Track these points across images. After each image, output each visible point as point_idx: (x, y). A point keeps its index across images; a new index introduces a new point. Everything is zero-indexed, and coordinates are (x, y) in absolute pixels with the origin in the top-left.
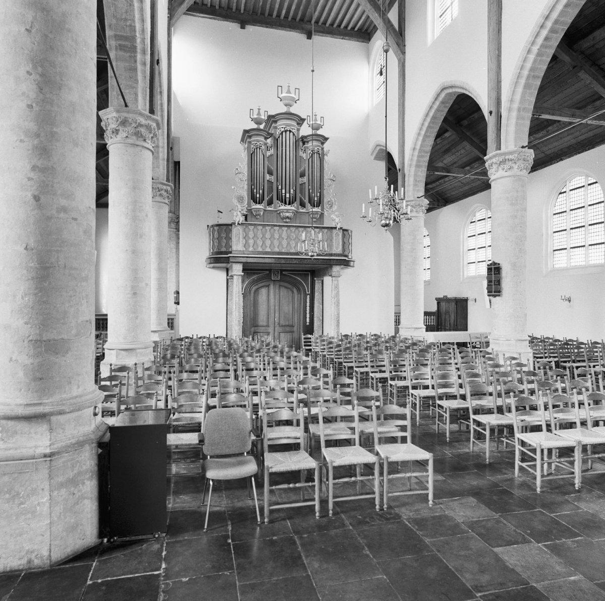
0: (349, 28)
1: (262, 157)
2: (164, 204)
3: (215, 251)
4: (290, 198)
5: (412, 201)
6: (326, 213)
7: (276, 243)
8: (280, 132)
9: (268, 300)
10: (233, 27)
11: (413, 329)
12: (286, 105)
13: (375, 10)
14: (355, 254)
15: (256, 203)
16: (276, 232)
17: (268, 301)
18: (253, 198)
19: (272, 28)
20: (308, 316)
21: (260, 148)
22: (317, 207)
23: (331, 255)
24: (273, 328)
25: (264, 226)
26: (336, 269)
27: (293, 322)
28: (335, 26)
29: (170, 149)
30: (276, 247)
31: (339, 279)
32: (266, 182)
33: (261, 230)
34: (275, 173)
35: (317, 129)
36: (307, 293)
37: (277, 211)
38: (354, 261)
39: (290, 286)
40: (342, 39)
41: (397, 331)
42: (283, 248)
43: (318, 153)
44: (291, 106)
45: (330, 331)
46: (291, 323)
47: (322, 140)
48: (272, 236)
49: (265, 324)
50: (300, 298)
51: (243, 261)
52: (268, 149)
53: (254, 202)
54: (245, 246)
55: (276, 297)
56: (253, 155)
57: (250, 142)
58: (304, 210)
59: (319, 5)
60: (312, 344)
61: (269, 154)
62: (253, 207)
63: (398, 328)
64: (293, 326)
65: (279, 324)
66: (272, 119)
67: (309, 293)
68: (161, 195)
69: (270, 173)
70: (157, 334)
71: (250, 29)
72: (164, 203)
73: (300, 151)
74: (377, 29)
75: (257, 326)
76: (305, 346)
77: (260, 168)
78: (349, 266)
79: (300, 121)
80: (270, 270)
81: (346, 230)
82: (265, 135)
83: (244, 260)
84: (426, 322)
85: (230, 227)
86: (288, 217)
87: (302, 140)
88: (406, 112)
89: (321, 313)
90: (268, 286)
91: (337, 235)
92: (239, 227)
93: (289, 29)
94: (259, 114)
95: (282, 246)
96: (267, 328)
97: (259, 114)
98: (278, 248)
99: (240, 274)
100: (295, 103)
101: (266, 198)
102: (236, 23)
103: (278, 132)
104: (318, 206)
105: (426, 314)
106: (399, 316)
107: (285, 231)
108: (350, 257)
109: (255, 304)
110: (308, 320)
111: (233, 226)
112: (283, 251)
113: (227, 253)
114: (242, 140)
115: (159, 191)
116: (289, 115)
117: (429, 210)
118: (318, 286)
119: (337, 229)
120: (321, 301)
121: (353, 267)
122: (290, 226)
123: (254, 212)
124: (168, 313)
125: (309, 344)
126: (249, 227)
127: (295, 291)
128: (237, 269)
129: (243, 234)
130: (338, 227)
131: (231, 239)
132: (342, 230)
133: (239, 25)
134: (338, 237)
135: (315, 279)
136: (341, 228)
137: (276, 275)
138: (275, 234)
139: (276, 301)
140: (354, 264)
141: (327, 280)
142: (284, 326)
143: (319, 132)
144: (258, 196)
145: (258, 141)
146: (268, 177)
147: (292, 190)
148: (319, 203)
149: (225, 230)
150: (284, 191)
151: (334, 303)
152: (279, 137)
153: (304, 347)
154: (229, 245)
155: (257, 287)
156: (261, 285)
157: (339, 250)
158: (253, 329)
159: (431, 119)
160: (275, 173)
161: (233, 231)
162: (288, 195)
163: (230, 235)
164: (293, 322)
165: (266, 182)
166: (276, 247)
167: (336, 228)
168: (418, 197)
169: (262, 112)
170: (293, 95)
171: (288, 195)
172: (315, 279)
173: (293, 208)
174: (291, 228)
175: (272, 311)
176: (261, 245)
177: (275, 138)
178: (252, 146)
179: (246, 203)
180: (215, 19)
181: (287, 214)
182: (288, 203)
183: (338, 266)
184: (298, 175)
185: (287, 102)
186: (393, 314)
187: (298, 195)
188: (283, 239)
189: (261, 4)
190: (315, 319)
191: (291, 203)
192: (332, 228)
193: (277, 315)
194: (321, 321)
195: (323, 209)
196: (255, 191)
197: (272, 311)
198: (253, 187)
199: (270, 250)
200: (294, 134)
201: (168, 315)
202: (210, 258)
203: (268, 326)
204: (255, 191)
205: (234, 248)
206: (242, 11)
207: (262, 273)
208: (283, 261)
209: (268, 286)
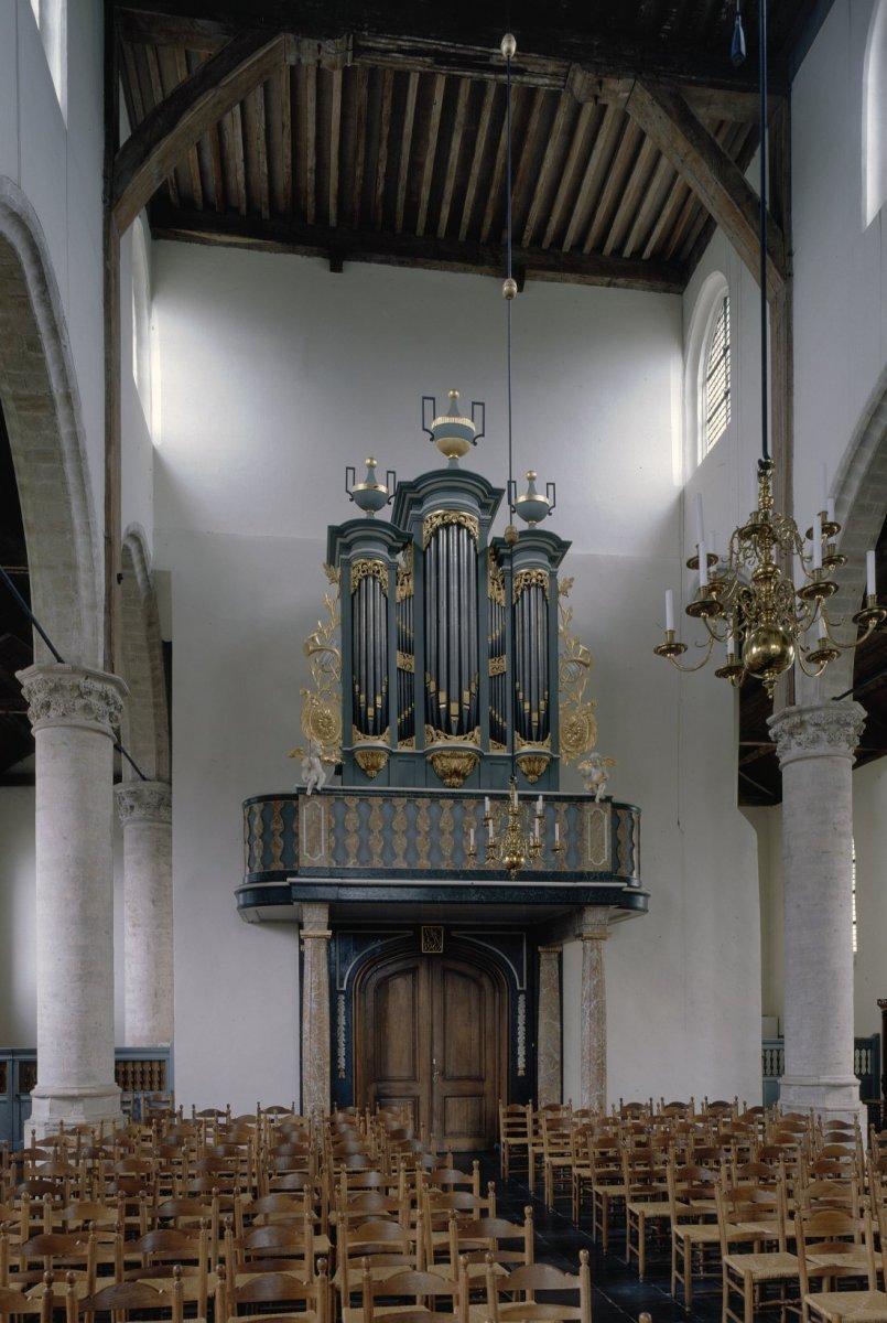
0: (627, 252)
1: (381, 601)
2: (98, 736)
3: (256, 870)
4: (460, 715)
5: (818, 709)
6: (564, 762)
7: (423, 845)
8: (431, 530)
9: (414, 1008)
10: (311, 267)
11: (823, 1089)
12: (447, 452)
13: (702, 154)
14: (647, 877)
15: (367, 732)
16: (423, 811)
17: (414, 1011)
18: (358, 719)
19: (414, 265)
20: (521, 1051)
21: (374, 578)
22: (538, 740)
23: (581, 876)
24: (426, 1086)
25: (388, 796)
26: (594, 917)
27: (481, 1069)
28: (587, 248)
29: (115, 579)
30: (423, 854)
31: (603, 944)
32: (394, 672)
33: (381, 807)
34: (418, 648)
35: (539, 519)
36: (518, 988)
37: (424, 755)
38: (646, 895)
39: (471, 971)
40: (609, 285)
41: (772, 1095)
42: (442, 857)
43: (539, 586)
44: (461, 453)
45: (578, 1094)
46: (474, 1072)
47: (551, 549)
48: (412, 827)
49: (405, 1074)
50: (501, 1005)
51: (330, 897)
52: (396, 580)
53: (360, 729)
54: (333, 856)
55: (435, 1004)
56: (356, 597)
57: (347, 564)
58: (504, 752)
59: (541, 180)
60: (507, 1130)
61: (403, 594)
62: (359, 744)
63: (777, 1086)
64: (480, 1079)
65: (443, 1073)
66: (409, 495)
67: (525, 988)
68: (87, 708)
69: (406, 647)
70: (80, 1107)
71: (356, 270)
72: (98, 731)
73: (490, 585)
74: (716, 224)
75: (385, 1079)
76: (509, 1135)
77: (376, 629)
78: (635, 908)
79: (489, 498)
80: (416, 928)
81: (625, 807)
82: (390, 541)
83: (330, 894)
84: (860, 1066)
85: (295, 803)
86: (456, 773)
87: (496, 552)
88: (796, 450)
89: (558, 1043)
90: (414, 971)
91: (597, 818)
92: (317, 801)
93: (460, 265)
94: (371, 479)
95: (440, 850)
96: (411, 1084)
97: (371, 479)
98: (429, 859)
99: (320, 933)
100: (471, 446)
101: (396, 720)
102: (317, 255)
103: (427, 529)
104: (541, 736)
105: (860, 1044)
106: (778, 1051)
107: (446, 809)
108: (635, 883)
109: (380, 1019)
110: (521, 1063)
111: (301, 797)
112: (443, 867)
113: (282, 876)
114: (331, 560)
115: (81, 696)
116: (455, 480)
117: (855, 767)
118: (546, 970)
119: (597, 800)
120: (557, 1011)
121: (645, 910)
122: (461, 796)
123: (359, 759)
124: (118, 1045)
125: (521, 1130)
126: (347, 799)
127: (486, 982)
128: (316, 921)
129: (330, 821)
130: (600, 793)
131: (297, 835)
132: (609, 805)
133: (327, 262)
134: (598, 825)
135: (540, 949)
136: (608, 799)
137: (432, 939)
138: (419, 820)
139: (435, 1013)
140: (646, 903)
141: (573, 951)
142: (459, 1079)
143: (540, 526)
144: (371, 711)
145: (370, 557)
146: (399, 659)
147: (466, 695)
148: (545, 729)
149: (281, 812)
150: (443, 697)
151: (591, 1015)
152: (429, 545)
153: (503, 1139)
154: (290, 853)
155: (381, 974)
156: (392, 969)
157: (603, 862)
158: (372, 1089)
159: (878, 451)
160: (418, 648)
161: (300, 811)
162: (454, 708)
163: (295, 825)
164: (481, 1069)
165: (394, 672)
166: (423, 854)
167: (591, 799)
168: (834, 699)
169: (380, 475)
170: (467, 422)
171: (454, 708)
172: (540, 949)
173: (471, 745)
174: (465, 802)
175: (425, 1041)
176: (379, 851)
177: (417, 548)
178: (354, 573)
179: (339, 734)
180: (259, 248)
181: (455, 764)
182: (454, 729)
183: (599, 908)
184: (485, 653)
185: (450, 440)
186: (759, 1047)
187: (486, 709)
188: (442, 832)
189: (381, 190)
190: (542, 1060)
191: (465, 730)
192: (582, 799)
193: (437, 1050)
194: (558, 1066)
195: (555, 747)
196: (363, 697)
197: (425, 1041)
198: (357, 686)
199: (404, 866)
200: (470, 536)
201: (118, 1051)
202: (244, 891)
203: (414, 1078)
204: (363, 697)
205: (307, 859)
206: (333, 221)
207: (398, 934)
208: (442, 897)
209: (414, 971)
